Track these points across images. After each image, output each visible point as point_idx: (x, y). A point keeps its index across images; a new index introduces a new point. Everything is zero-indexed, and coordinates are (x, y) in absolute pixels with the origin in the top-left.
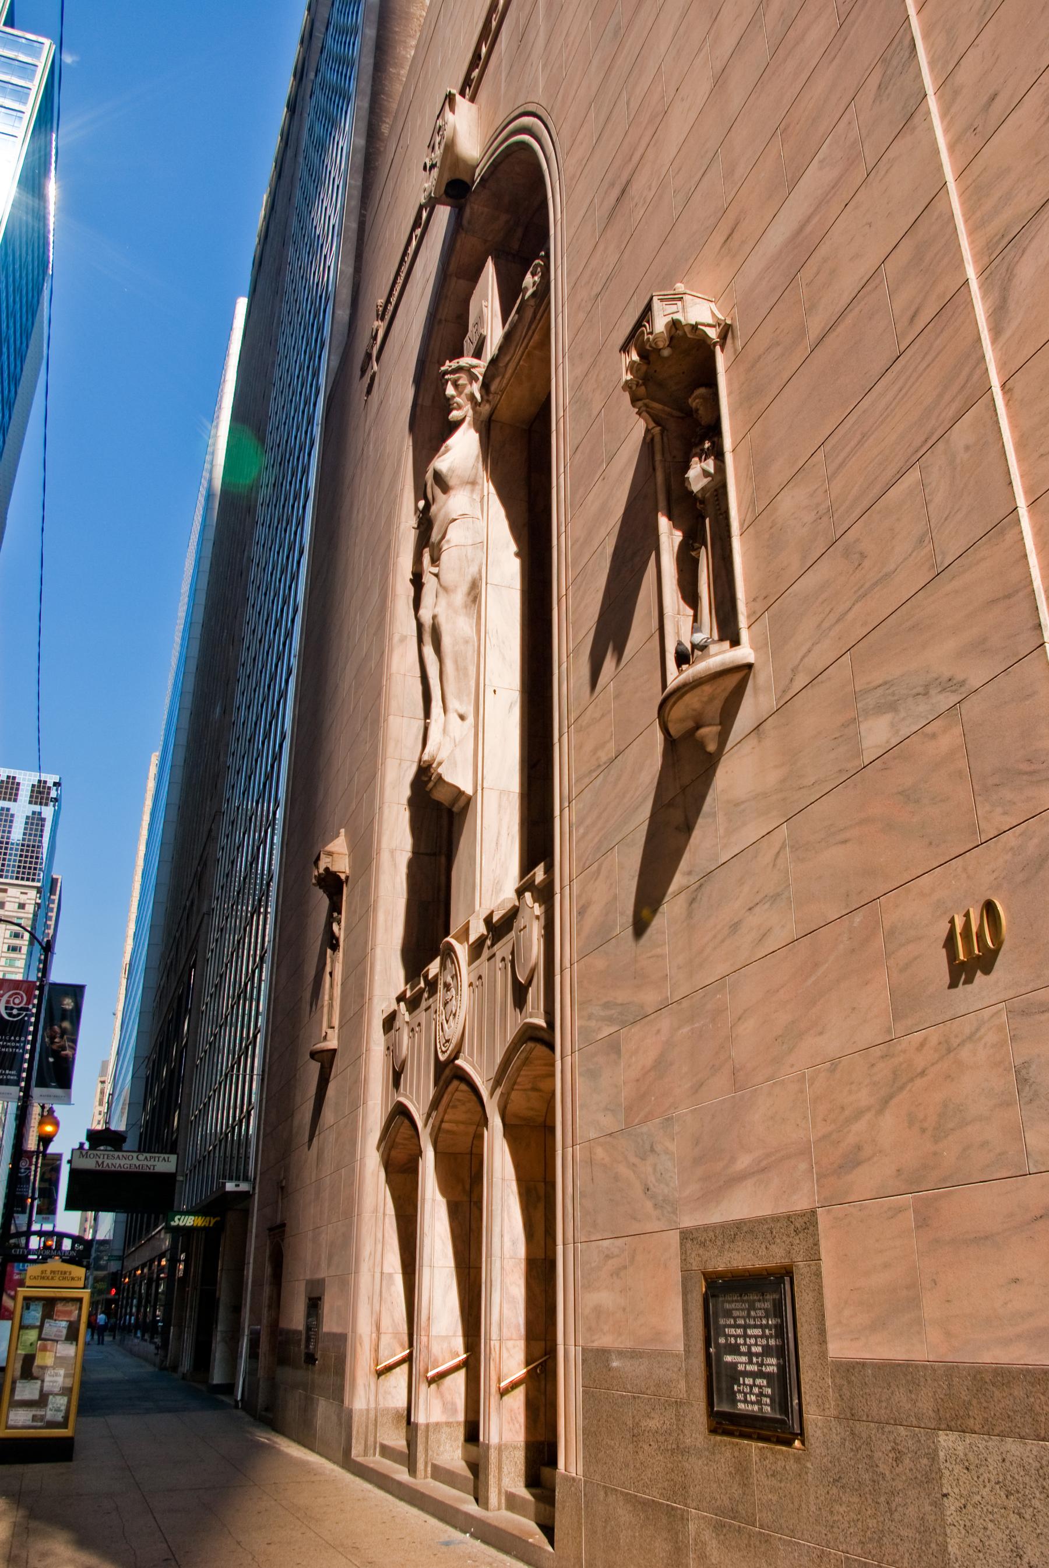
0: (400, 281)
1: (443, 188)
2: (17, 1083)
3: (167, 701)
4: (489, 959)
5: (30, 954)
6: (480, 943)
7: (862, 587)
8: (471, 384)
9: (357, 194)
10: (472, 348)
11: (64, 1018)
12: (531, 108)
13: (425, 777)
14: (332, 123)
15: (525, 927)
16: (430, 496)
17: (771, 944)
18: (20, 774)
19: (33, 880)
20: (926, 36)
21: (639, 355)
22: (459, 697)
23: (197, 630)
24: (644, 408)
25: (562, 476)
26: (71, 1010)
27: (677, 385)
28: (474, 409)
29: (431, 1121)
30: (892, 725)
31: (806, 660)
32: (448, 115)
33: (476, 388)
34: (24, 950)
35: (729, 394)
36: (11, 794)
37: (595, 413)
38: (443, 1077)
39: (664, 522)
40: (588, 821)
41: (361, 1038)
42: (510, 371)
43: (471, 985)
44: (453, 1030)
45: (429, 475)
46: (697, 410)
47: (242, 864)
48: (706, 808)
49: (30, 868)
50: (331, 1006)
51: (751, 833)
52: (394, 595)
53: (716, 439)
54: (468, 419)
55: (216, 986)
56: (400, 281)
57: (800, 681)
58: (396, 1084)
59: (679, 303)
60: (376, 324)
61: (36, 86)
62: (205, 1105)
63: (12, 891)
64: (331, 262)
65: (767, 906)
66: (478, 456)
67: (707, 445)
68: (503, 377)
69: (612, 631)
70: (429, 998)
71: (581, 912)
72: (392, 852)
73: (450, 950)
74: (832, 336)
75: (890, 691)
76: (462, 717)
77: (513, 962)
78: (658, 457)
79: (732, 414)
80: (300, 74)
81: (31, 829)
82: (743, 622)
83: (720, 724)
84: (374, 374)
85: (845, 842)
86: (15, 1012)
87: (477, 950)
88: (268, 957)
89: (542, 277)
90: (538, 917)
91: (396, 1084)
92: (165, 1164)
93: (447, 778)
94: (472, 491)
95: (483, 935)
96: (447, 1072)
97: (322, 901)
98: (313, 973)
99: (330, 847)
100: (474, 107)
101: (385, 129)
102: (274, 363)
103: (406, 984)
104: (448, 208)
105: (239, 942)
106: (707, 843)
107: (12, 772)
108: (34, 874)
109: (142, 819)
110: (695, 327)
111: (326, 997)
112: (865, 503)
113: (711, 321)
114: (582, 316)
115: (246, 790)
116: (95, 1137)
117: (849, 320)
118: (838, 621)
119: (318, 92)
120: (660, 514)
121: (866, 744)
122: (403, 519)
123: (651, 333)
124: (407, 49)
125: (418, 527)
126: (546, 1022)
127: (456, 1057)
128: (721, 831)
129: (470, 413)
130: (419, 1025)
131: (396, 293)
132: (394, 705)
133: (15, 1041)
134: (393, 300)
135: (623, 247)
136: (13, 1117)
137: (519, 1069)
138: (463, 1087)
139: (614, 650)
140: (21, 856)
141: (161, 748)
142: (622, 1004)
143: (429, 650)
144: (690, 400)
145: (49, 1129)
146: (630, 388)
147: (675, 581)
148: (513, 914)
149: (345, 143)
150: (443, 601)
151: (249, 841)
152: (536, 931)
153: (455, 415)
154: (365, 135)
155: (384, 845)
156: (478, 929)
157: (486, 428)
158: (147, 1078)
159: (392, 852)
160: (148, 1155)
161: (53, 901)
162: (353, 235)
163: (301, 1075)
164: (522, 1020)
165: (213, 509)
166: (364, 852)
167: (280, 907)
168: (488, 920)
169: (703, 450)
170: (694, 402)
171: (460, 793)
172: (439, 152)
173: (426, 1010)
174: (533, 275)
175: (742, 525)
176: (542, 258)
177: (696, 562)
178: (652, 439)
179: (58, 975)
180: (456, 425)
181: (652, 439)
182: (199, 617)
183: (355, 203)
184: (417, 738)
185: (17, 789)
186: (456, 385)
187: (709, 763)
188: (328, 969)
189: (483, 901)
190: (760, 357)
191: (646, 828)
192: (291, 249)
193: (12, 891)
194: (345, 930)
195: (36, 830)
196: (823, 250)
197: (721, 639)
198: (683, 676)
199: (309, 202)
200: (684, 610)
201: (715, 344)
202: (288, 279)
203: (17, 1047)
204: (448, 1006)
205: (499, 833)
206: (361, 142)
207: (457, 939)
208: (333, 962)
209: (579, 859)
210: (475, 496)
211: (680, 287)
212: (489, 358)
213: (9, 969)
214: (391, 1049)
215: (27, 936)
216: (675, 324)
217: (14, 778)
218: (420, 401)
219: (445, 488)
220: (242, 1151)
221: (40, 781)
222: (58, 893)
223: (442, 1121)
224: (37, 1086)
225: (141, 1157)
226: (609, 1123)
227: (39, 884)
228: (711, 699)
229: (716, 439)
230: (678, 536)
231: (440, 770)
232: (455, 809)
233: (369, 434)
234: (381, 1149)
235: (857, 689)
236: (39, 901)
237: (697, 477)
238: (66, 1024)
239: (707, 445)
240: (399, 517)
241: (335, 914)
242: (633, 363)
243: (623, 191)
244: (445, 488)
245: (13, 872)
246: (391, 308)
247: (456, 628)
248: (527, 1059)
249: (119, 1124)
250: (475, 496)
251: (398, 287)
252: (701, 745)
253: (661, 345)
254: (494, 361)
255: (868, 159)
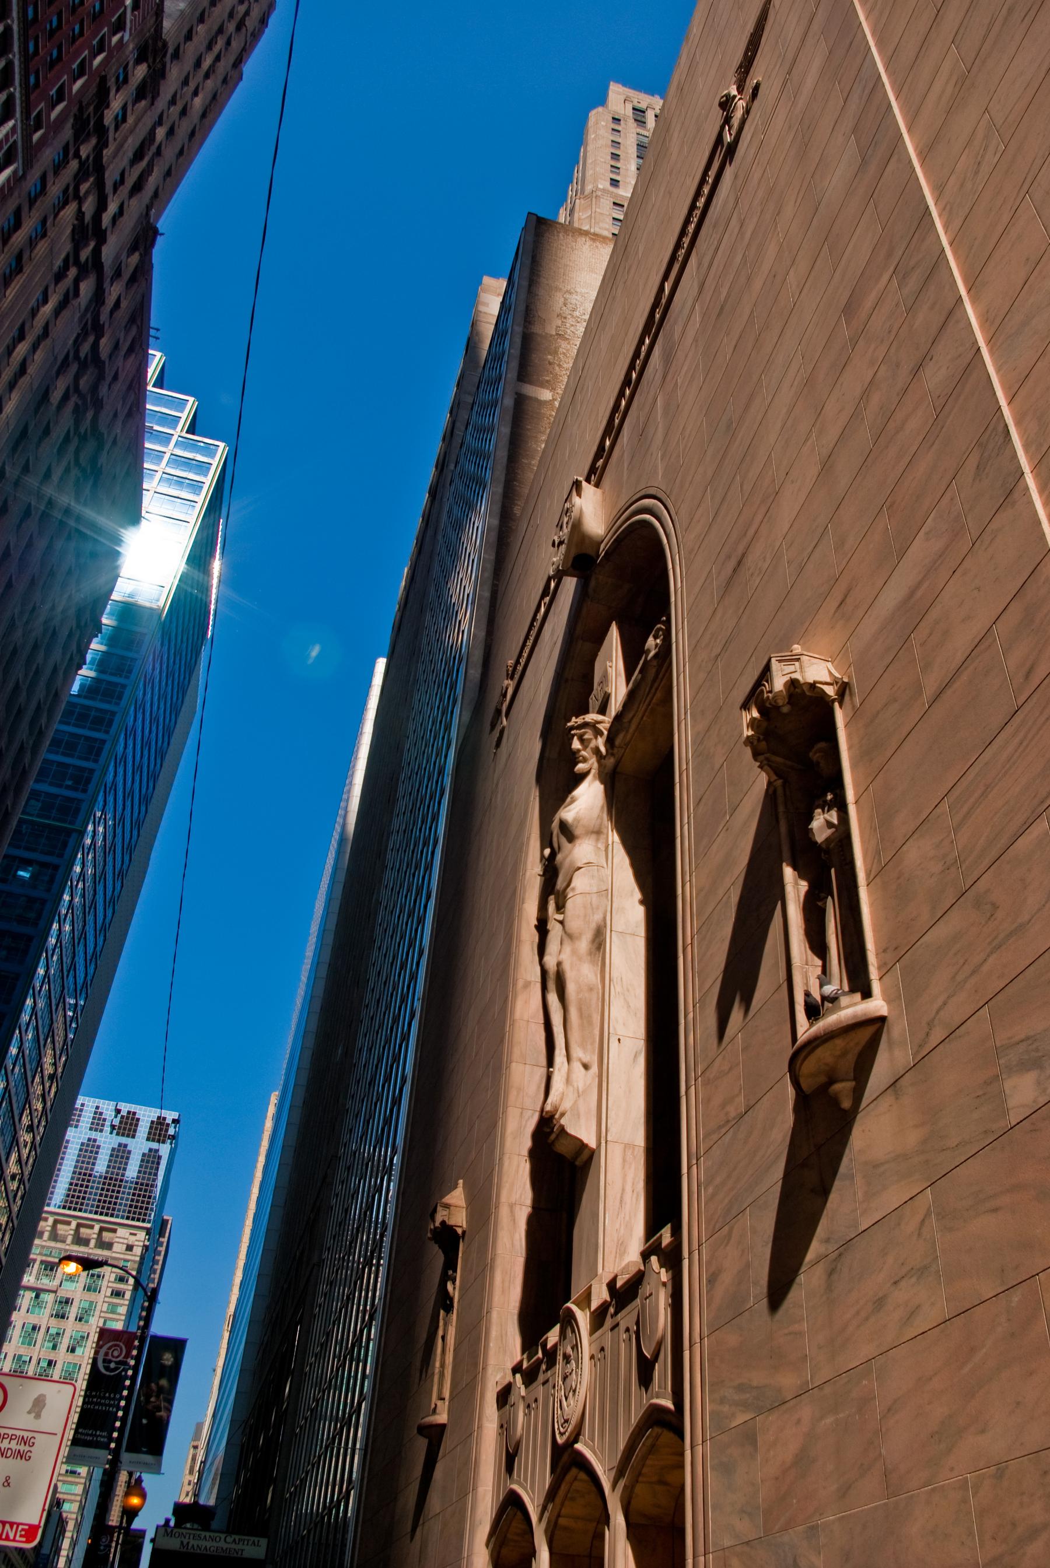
0: (529, 643)
1: (570, 564)
2: (106, 1446)
3: (290, 1040)
4: (612, 1329)
5: (133, 1299)
6: (603, 1308)
7: (996, 938)
8: (596, 738)
9: (490, 567)
10: (597, 704)
11: (161, 1376)
12: (652, 491)
13: (547, 1129)
14: (470, 506)
15: (651, 1295)
16: (556, 845)
17: (921, 1324)
18: (140, 1110)
19: (144, 1221)
20: (1018, 423)
21: (759, 712)
22: (583, 1046)
23: (324, 972)
24: (765, 762)
25: (686, 827)
26: (171, 1367)
27: (797, 739)
28: (599, 761)
29: (546, 1515)
30: (1039, 1083)
31: (942, 1013)
32: (576, 499)
33: (601, 743)
34: (128, 1295)
35: (850, 748)
36: (130, 1130)
37: (717, 766)
38: (561, 1464)
39: (788, 872)
40: (718, 1180)
41: (473, 1411)
42: (633, 727)
43: (592, 1357)
44: (572, 1408)
45: (555, 825)
46: (818, 763)
47: (356, 1211)
48: (843, 1169)
49: (141, 1208)
50: (442, 1375)
51: (893, 1197)
52: (519, 941)
53: (838, 791)
54: (593, 771)
55: (322, 1345)
56: (529, 643)
57: (938, 1034)
58: (510, 1469)
59: (797, 664)
60: (506, 682)
61: (209, 481)
62: (301, 1480)
63: (122, 1232)
64: (465, 626)
65: (914, 1279)
66: (602, 807)
67: (829, 797)
68: (627, 731)
69: (739, 981)
70: (547, 1370)
71: (712, 1280)
72: (511, 1206)
73: (569, 1320)
74: (949, 692)
75: (1034, 1046)
76: (586, 1067)
77: (637, 1333)
78: (781, 809)
79: (853, 767)
80: (441, 465)
81: (146, 1167)
82: (874, 973)
83: (855, 1079)
84: (504, 728)
85: (995, 1210)
86: (112, 1365)
87: (598, 1318)
88: (379, 1316)
89: (663, 640)
90: (664, 1284)
91: (510, 1469)
92: (255, 1549)
93: (571, 1130)
94: (597, 840)
95: (606, 1301)
96: (565, 1458)
97: (437, 1257)
98: (424, 1336)
99: (448, 1199)
100: (599, 491)
101: (517, 510)
102: (408, 717)
103: (523, 1353)
104: (575, 579)
105: (348, 1297)
106: (845, 1208)
107: (133, 1108)
108: (145, 1215)
109: (257, 1161)
110: (813, 686)
111: (438, 1364)
112: (994, 853)
113: (828, 680)
114: (702, 676)
115: (365, 1133)
116: (180, 1510)
117: (964, 677)
118: (973, 972)
119: (457, 480)
120: (784, 864)
121: (1012, 1103)
122: (529, 866)
123: (771, 692)
124: (539, 444)
125: (544, 875)
126: (674, 1404)
127: (576, 1441)
128: (860, 1195)
129: (596, 765)
130: (536, 1400)
131: (525, 655)
132: (516, 1052)
133: (109, 1398)
134: (523, 661)
135: (741, 611)
136: (98, 1484)
137: (644, 1458)
138: (583, 1476)
139: (742, 1000)
140: (134, 1195)
141: (281, 1087)
142: (757, 1387)
143: (553, 998)
144: (811, 754)
145: (135, 1501)
146: (752, 743)
147: (802, 932)
148: (638, 1280)
149: (479, 526)
150: (567, 949)
151: (364, 1188)
152: (663, 1299)
153: (581, 767)
154: (498, 516)
155: (504, 1198)
156: (600, 1295)
157: (611, 780)
158: (243, 1446)
159: (511, 1206)
160: (237, 1537)
161: (161, 1244)
162: (486, 604)
163: (409, 1451)
164: (648, 1400)
165: (345, 852)
166: (483, 1207)
167: (393, 1261)
168: (611, 1285)
169: (825, 802)
170: (815, 756)
171: (583, 1146)
172: (566, 530)
173: (544, 1384)
174: (656, 637)
175: (868, 875)
176: (663, 623)
177: (823, 912)
178: (775, 791)
179: (160, 1327)
180: (581, 777)
181: (775, 791)
182: (327, 957)
183: (489, 574)
184: (539, 1087)
185: (136, 1125)
186: (581, 740)
187: (844, 1122)
188: (440, 1333)
189: (606, 1240)
190: (878, 713)
191: (779, 1190)
192: (428, 617)
193: (122, 1232)
194: (460, 1290)
195: (152, 1168)
196: (934, 614)
197: (852, 990)
198: (814, 1029)
199: (446, 574)
200: (813, 960)
201: (834, 701)
202: (424, 641)
203: (110, 1405)
204: (568, 1380)
205: (623, 1190)
206: (496, 522)
207: (577, 1305)
208: (446, 1325)
209: (708, 1223)
210: (600, 845)
211: (797, 648)
212: (613, 714)
213: (111, 1316)
214: (505, 1427)
215: (131, 1281)
216: (793, 683)
217: (134, 1113)
218: (547, 754)
219: (571, 837)
220: (339, 1536)
221: (159, 1118)
222: (167, 1235)
223: (559, 1516)
224: (127, 1450)
225: (229, 1539)
226: (745, 1528)
227: (149, 1225)
228: (844, 1054)
229: (838, 791)
230: (804, 886)
231: (563, 1122)
232: (577, 1163)
233: (497, 785)
234: (491, 1545)
235: (998, 1045)
236: (147, 1243)
237: (820, 828)
238: (164, 1382)
239: (829, 797)
240: (525, 863)
241: (450, 1272)
242: (753, 720)
243: (739, 563)
244: (571, 837)
245: (124, 1211)
246: (520, 668)
247: (580, 975)
248: (653, 1446)
249: (209, 1499)
250: (600, 845)
251: (527, 650)
252: (835, 1101)
253: (780, 702)
254: (618, 718)
255: (972, 531)
